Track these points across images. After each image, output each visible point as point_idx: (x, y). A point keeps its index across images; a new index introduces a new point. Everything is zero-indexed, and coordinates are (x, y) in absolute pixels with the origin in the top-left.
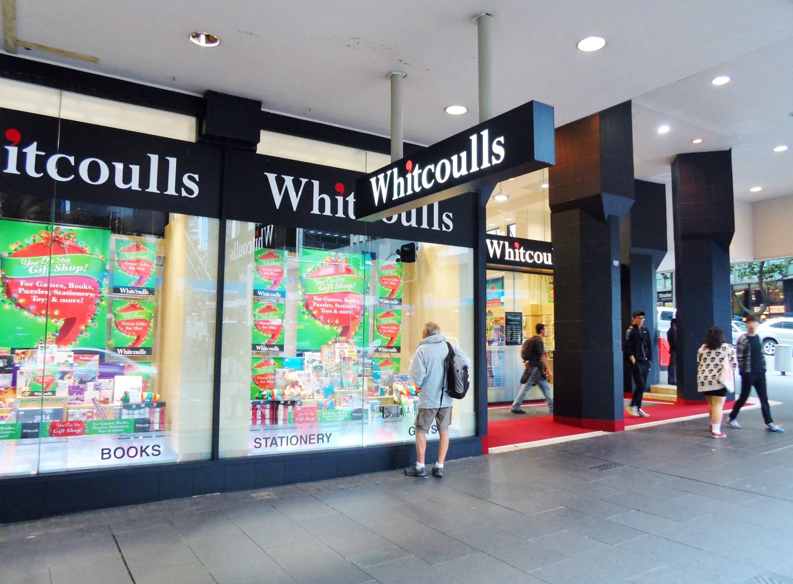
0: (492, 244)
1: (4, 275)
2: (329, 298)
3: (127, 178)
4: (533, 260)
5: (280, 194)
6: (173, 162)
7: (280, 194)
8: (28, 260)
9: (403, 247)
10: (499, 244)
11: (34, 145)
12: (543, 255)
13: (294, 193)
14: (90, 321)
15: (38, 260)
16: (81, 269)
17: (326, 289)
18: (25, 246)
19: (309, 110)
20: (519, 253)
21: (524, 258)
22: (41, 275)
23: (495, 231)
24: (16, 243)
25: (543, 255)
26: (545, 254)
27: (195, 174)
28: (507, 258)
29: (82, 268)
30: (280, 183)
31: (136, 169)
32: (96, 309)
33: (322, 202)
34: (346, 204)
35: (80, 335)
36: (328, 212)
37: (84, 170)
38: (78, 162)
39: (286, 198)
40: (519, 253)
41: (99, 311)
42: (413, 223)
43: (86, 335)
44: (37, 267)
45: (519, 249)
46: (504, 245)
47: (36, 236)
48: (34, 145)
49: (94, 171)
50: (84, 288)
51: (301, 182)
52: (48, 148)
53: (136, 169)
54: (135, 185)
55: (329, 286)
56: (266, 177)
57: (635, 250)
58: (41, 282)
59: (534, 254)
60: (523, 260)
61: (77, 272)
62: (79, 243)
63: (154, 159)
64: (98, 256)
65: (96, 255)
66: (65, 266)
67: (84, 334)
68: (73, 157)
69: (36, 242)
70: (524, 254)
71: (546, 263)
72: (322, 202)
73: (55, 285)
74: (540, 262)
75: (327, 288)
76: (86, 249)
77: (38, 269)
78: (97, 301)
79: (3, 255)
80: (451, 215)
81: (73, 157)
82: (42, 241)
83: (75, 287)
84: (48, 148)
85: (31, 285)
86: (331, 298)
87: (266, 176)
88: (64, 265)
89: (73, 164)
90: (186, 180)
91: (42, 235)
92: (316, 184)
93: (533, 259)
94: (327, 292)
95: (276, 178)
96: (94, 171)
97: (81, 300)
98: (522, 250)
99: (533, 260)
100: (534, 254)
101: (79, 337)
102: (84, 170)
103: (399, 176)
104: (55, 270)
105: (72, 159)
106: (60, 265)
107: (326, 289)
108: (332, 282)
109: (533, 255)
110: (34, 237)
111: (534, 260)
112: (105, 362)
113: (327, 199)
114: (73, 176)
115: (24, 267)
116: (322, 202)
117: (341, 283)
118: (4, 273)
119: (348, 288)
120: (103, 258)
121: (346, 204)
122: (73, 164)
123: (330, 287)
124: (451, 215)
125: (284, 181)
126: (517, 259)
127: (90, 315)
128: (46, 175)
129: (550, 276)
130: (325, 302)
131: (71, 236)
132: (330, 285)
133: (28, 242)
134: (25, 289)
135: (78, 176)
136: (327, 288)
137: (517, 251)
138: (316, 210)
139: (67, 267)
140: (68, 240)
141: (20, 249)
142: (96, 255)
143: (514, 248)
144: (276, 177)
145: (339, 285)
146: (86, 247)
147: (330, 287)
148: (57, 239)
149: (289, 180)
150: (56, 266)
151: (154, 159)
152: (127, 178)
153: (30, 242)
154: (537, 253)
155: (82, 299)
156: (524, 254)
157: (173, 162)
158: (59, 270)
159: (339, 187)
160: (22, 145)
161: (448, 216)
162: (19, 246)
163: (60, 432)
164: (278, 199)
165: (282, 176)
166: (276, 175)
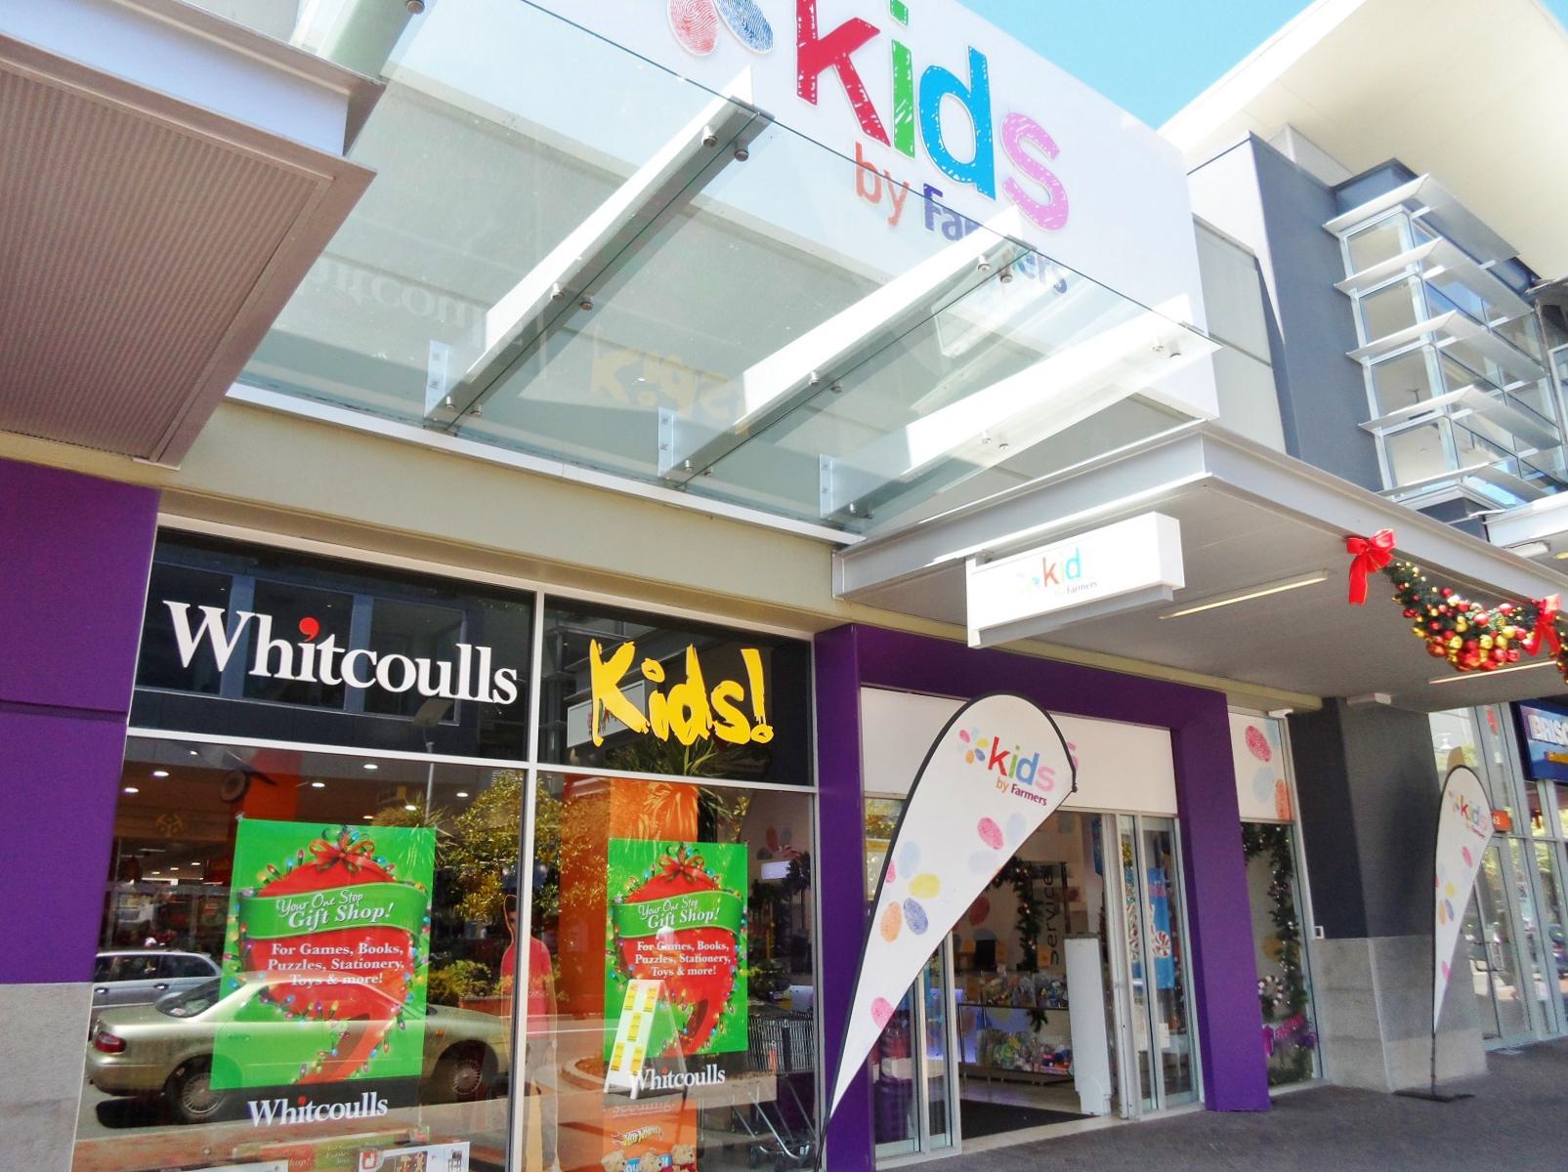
0: (259, 1107)
1: (245, 933)
2: (314, 945)
3: (434, 682)
4: (278, 642)
6: (374, 1095)
8: (287, 900)
10: (272, 1105)
12: (417, 666)
14: (726, 1004)
15: (307, 900)
16: (381, 914)
17: (308, 924)
18: (283, 873)
21: (336, 672)
22: (310, 929)
24: (269, 867)
25: (417, 666)
27: (371, 650)
29: (382, 910)
30: (195, 619)
32: (732, 982)
33: (275, 656)
34: (318, 654)
35: (375, 1051)
36: (285, 672)
39: (205, 648)
41: (736, 987)
43: (386, 1051)
44: (303, 914)
47: (304, 852)
49: (396, 673)
50: (386, 952)
53: (445, 667)
55: (667, 918)
56: (167, 609)
58: (310, 945)
59: (378, 661)
60: (327, 678)
61: (706, 922)
62: (379, 860)
63: (365, 1095)
64: (413, 885)
65: (409, 883)
66: (354, 909)
67: (382, 1047)
68: (375, 653)
69: (304, 862)
70: (337, 659)
71: (425, 689)
72: (275, 656)
73: (335, 948)
74: (406, 685)
75: (313, 920)
76: (392, 872)
77: (304, 917)
78: (733, 969)
79: (245, 894)
81: (375, 653)
82: (315, 861)
83: (370, 952)
85: (291, 953)
86: (321, 946)
87: (167, 607)
88: (352, 906)
91: (315, 849)
93: (375, 677)
94: (310, 930)
96: (396, 673)
97: (379, 976)
99: (340, 680)
100: (378, 661)
101: (372, 1056)
104: (337, 919)
106: (345, 907)
107: (308, 924)
108: (673, 908)
109: (374, 663)
110: (301, 852)
111: (377, 683)
115: (280, 916)
117: (691, 910)
118: (244, 930)
119: (371, 916)
120: (421, 888)
121: (318, 654)
123: (320, 918)
125: (202, 615)
126: (306, 675)
127: (725, 995)
130: (304, 957)
131: (365, 847)
132: (670, 916)
133: (290, 864)
134: (280, 962)
136: (313, 920)
137: (308, 650)
138: (261, 669)
139: (356, 911)
140: (361, 855)
141: (276, 878)
142: (409, 883)
143: (295, 639)
144: (188, 610)
145: (687, 915)
146: (392, 867)
147: (320, 918)
148: (342, 855)
149: (266, 1104)
150: (339, 911)
152: (434, 682)
153: (292, 863)
154: (388, 660)
155: (715, 967)
156: (337, 659)
158: (343, 915)
162: (274, 874)
164: (187, 649)
165: (200, 607)
166: (188, 605)
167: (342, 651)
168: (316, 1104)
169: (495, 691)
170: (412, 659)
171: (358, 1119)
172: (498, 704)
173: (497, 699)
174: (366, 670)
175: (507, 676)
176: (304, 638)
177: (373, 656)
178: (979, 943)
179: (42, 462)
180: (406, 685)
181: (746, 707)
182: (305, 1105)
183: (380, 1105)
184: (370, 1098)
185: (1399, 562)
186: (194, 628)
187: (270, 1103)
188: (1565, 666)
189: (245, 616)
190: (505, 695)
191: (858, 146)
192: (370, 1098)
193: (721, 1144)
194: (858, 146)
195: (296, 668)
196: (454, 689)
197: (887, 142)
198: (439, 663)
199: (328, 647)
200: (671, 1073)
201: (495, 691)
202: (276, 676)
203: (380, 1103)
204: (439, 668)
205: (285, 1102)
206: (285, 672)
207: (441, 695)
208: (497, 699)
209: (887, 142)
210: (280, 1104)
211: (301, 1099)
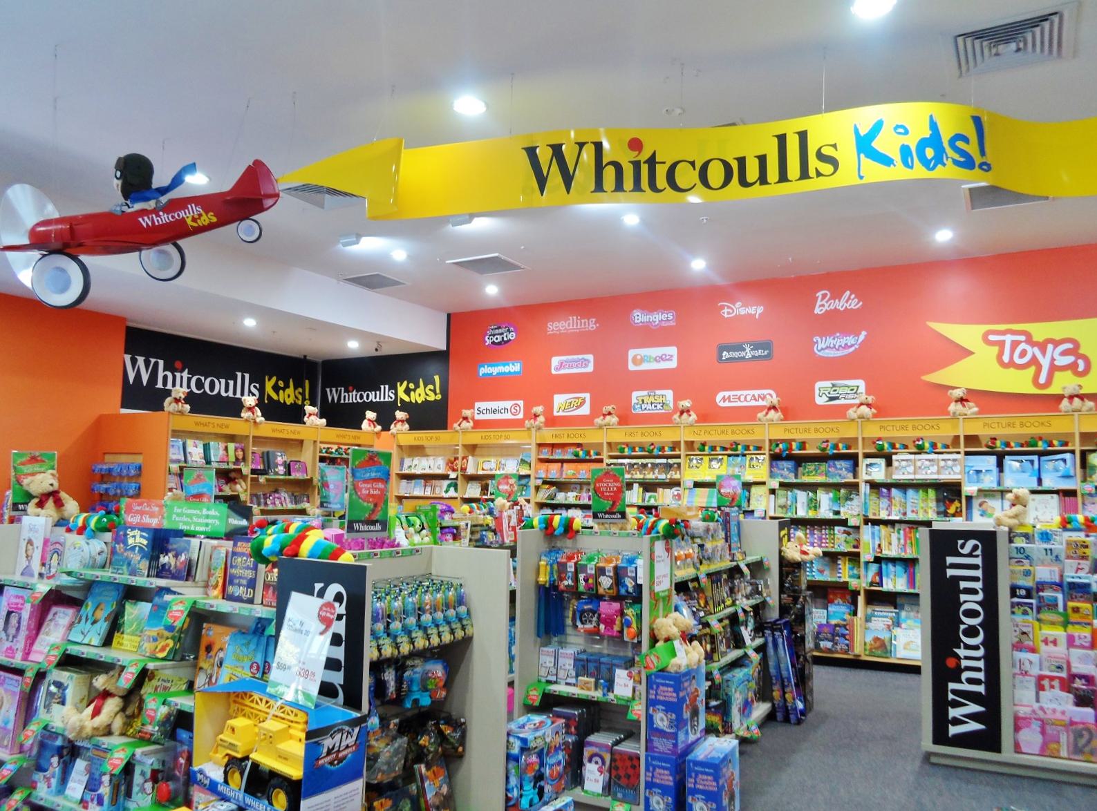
0: (956, 722)
3: (974, 592)
4: (963, 680)
5: (968, 705)
6: (950, 560)
7: (968, 705)
9: (357, 242)
12: (965, 602)
19: (1044, 552)
20: (182, 377)
21: (976, 648)
23: (560, 464)
25: (965, 602)
26: (963, 597)
30: (956, 722)
36: (981, 676)
37: (176, 215)
39: (974, 717)
40: (182, 377)
42: (230, 394)
45: (182, 371)
46: (156, 364)
49: (971, 614)
51: (150, 361)
59: (965, 624)
60: (981, 652)
63: (950, 572)
68: (316, 584)
70: (967, 647)
71: (980, 597)
72: (971, 681)
74: (216, 392)
80: (257, 385)
81: (316, 584)
92: (161, 363)
93: (204, 388)
95: (145, 360)
96: (971, 614)
100: (965, 624)
102: (176, 215)
116: (165, 378)
124: (257, 385)
125: (136, 360)
129: (506, 551)
138: (981, 689)
149: (953, 713)
152: (974, 592)
154: (209, 380)
156: (967, 647)
161: (255, 387)
164: (974, 726)
167: (962, 644)
169: (974, 554)
170: (961, 604)
171: (984, 584)
172: (982, 551)
173: (979, 552)
174: (971, 632)
175: (963, 546)
176: (959, 665)
177: (203, 378)
180: (978, 608)
181: (434, 391)
182: (958, 658)
183: (966, 550)
187: (953, 707)
189: (951, 696)
190: (975, 548)
191: (664, 163)
194: (664, 163)
195: (978, 670)
196: (976, 579)
197: (695, 169)
198: (961, 588)
201: (974, 554)
202: (983, 680)
203: (962, 551)
204: (965, 589)
205: (952, 686)
206: (981, 676)
207: (981, 587)
208: (979, 552)
209: (695, 169)
210: (954, 692)
211: (951, 663)
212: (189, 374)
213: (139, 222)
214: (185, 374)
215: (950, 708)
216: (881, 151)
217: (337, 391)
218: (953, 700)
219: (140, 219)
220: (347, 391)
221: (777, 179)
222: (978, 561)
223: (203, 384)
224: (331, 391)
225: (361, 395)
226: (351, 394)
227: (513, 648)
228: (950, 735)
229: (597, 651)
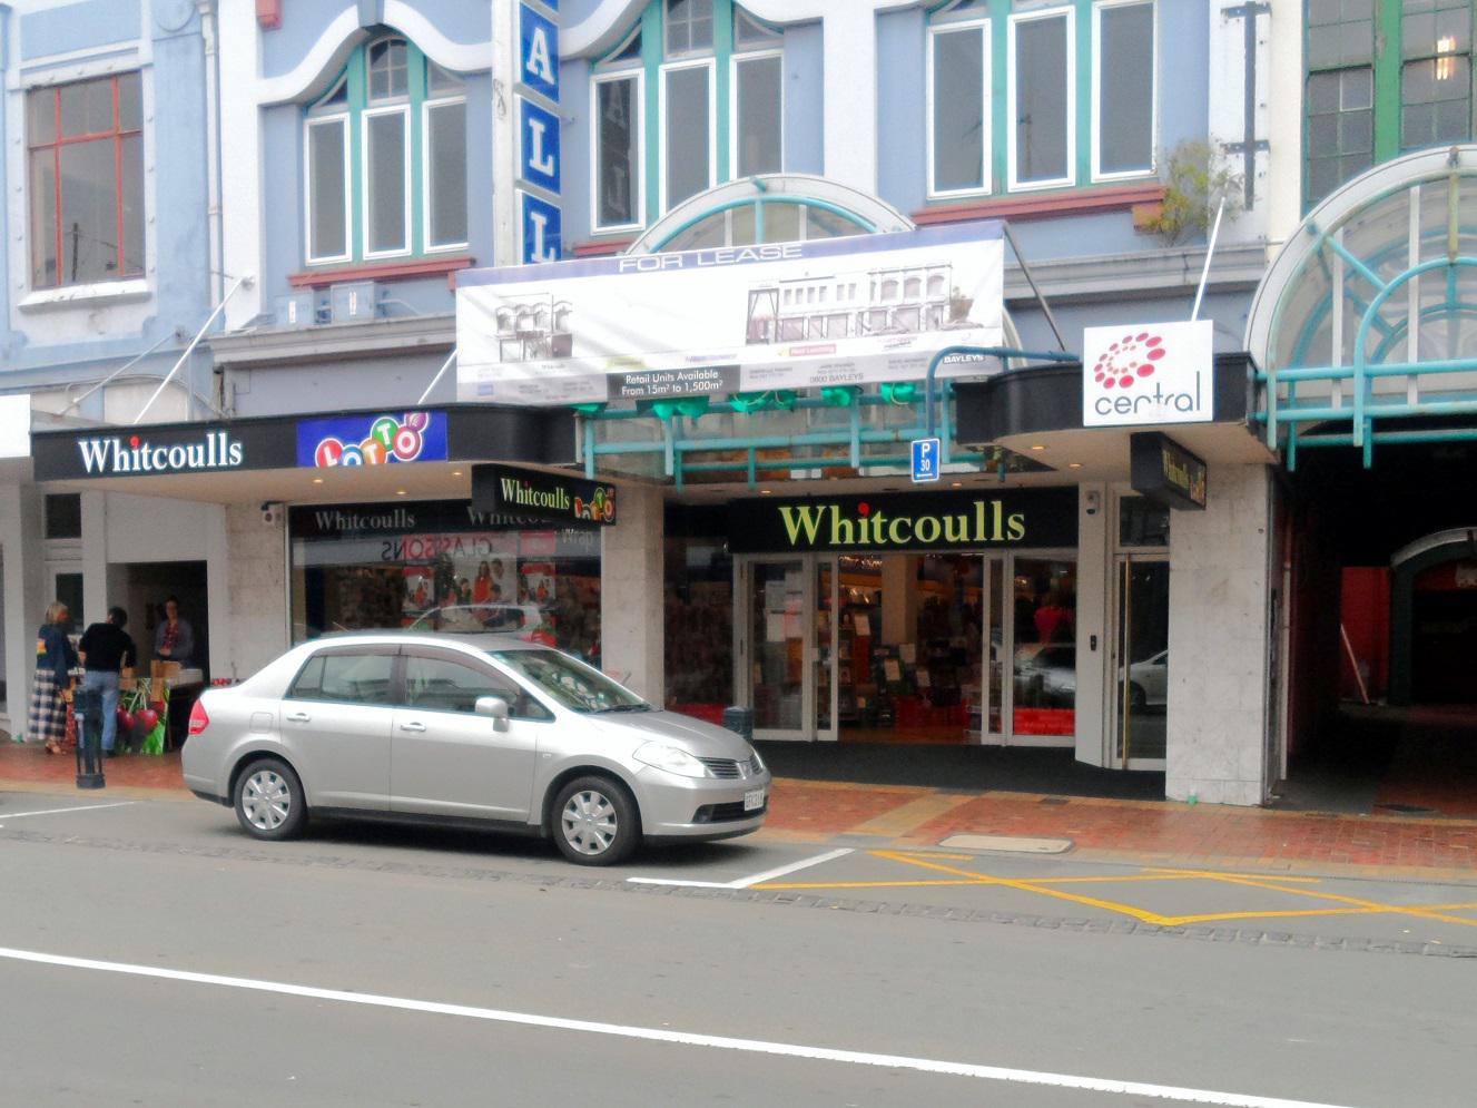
0: (795, 515)
3: (956, 530)
10: (813, 514)
11: (879, 514)
13: (792, 525)
27: (906, 517)
28: (117, 468)
30: (795, 515)
31: (963, 520)
33: (842, 530)
34: (871, 527)
36: (849, 539)
38: (914, 523)
39: (802, 533)
48: (879, 514)
49: (928, 529)
52: (889, 515)
53: (963, 520)
54: (963, 536)
57: (1068, 645)
60: (147, 467)
70: (150, 456)
71: (192, 464)
72: (842, 530)
80: (1022, 517)
84: (889, 515)
89: (910, 524)
90: (1011, 522)
96: (928, 529)
98: (878, 520)
103: (843, 515)
105: (909, 521)
112: (879, 232)
113: (848, 524)
114: (909, 538)
121: (871, 527)
122: (910, 524)
126: (137, 467)
128: (890, 540)
135: (914, 536)
137: (864, 522)
138: (835, 540)
151: (980, 506)
152: (956, 530)
156: (150, 456)
157: (403, 512)
159: (863, 507)
160: (870, 516)
163: (660, 378)
164: (793, 533)
168: (360, 516)
173: (1010, 537)
174: (163, 458)
175: (1016, 519)
176: (861, 516)
177: (165, 451)
178: (37, 437)
179: (82, 510)
184: (218, 441)
185: (456, 469)
186: (795, 519)
188: (1294, 476)
189: (107, 442)
190: (1015, 533)
192: (218, 441)
193: (644, 582)
199: (145, 450)
200: (146, 446)
203: (232, 448)
204: (986, 535)
212: (883, 517)
213: (79, 450)
214: (530, 491)
215: (879, 513)
216: (1178, 1098)
217: (102, 446)
218: (817, 511)
219: (503, 480)
220: (523, 487)
221: (770, 323)
222: (223, 462)
223: (168, 457)
224: (90, 447)
225: (161, 454)
226: (136, 453)
227: (956, 358)
228: (781, 509)
229: (878, 488)
